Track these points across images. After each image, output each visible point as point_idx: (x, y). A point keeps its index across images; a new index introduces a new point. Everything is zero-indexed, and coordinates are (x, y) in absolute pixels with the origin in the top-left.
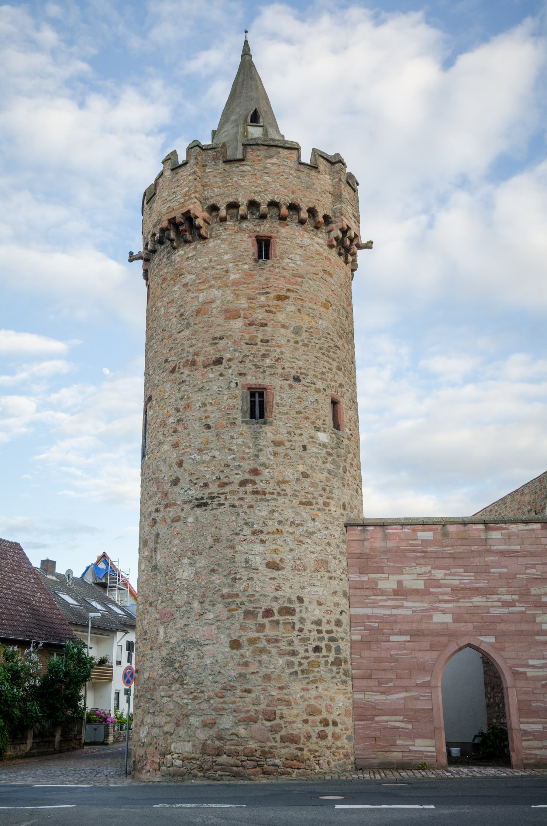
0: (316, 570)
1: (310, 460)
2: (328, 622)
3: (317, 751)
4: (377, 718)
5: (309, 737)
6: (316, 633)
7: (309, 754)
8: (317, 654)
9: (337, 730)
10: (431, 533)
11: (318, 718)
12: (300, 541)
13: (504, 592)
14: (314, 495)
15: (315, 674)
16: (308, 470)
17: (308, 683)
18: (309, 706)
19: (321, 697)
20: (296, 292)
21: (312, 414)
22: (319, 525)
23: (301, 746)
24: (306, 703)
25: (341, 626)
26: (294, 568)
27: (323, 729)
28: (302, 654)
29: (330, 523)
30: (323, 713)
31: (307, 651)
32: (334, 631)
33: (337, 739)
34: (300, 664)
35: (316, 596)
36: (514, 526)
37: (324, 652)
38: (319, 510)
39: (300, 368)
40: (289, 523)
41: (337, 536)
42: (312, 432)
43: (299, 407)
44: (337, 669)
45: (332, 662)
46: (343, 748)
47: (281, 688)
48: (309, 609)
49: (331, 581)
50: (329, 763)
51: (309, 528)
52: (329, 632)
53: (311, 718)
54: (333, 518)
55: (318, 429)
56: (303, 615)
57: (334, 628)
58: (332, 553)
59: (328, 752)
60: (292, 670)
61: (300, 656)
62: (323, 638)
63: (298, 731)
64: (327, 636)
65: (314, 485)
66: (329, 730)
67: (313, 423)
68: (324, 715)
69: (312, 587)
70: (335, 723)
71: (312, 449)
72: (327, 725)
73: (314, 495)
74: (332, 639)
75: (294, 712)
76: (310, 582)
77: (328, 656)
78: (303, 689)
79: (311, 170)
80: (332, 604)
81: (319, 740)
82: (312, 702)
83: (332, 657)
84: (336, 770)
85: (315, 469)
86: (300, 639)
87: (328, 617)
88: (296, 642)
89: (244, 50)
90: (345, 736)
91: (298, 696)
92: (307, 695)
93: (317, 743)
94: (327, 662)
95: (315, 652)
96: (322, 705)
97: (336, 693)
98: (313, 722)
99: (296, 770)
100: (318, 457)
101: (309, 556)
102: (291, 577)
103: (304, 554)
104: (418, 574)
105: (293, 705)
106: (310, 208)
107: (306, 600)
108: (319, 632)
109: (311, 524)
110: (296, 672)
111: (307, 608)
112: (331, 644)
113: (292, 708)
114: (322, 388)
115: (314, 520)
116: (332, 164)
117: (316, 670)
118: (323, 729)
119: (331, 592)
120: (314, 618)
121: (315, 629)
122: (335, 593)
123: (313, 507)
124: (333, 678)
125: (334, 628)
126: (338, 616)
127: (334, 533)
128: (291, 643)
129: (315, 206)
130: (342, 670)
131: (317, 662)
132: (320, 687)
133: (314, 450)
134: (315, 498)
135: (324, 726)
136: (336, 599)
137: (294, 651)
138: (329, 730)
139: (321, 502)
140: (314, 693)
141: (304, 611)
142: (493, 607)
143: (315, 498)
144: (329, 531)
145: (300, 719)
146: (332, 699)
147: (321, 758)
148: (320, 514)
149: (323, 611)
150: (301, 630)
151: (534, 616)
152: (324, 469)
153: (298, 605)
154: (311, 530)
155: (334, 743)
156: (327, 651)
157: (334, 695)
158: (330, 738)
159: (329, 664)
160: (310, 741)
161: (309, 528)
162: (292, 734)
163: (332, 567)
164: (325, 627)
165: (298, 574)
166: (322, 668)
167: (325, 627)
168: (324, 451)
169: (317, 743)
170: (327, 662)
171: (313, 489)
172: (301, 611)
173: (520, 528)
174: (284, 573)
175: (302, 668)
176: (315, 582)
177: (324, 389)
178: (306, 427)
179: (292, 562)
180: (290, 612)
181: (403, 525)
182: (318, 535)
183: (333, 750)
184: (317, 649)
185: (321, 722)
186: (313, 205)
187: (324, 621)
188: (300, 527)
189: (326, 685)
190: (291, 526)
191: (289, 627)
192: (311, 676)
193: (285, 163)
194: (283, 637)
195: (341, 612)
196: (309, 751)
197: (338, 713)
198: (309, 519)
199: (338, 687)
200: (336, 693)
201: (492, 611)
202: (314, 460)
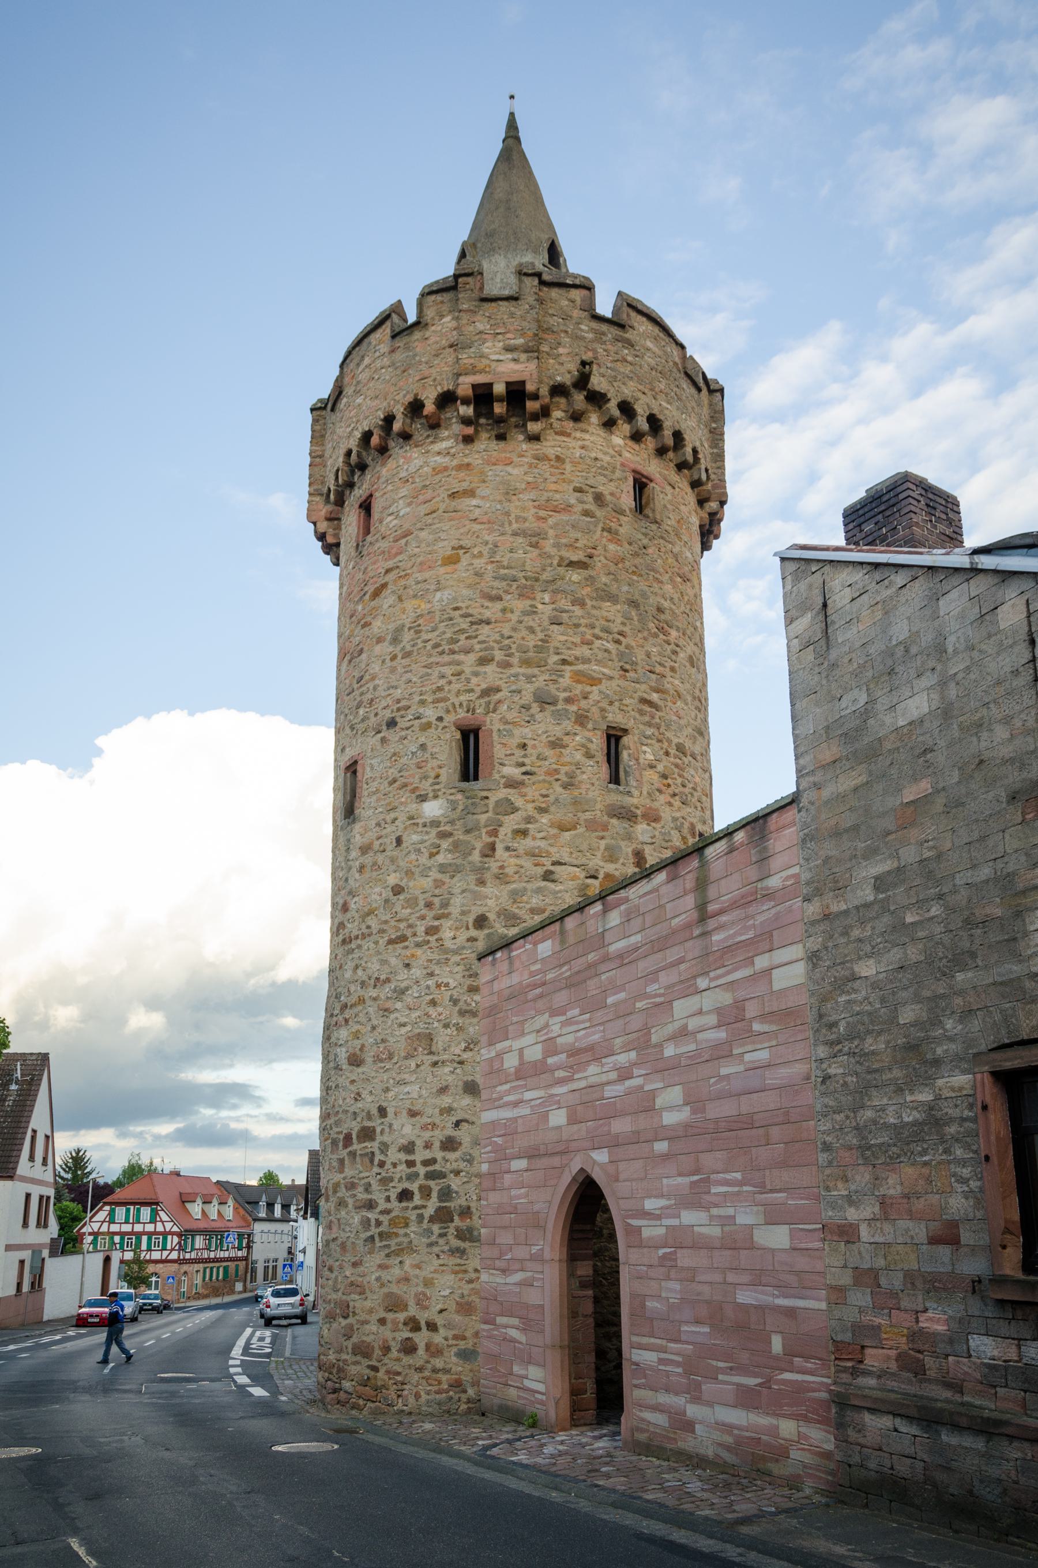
2: (428, 1146)
3: (399, 1374)
4: (500, 1320)
5: (386, 1349)
6: (403, 1167)
7: (386, 1377)
8: (404, 1204)
9: (438, 1339)
10: (549, 943)
11: (401, 1316)
12: (386, 1010)
13: (622, 1048)
17: (388, 1255)
18: (390, 1295)
21: (413, 776)
22: (417, 972)
23: (374, 1363)
24: (385, 1290)
25: (454, 1149)
28: (382, 1205)
29: (438, 963)
30: (410, 1308)
31: (388, 1199)
32: (439, 1159)
34: (378, 1223)
37: (417, 1200)
39: (398, 701)
41: (452, 984)
42: (413, 807)
43: (393, 773)
44: (440, 1228)
45: (431, 1217)
48: (395, 1127)
50: (417, 1396)
52: (426, 1163)
53: (390, 1316)
54: (446, 951)
55: (423, 798)
56: (386, 1138)
57: (439, 1155)
59: (416, 1377)
61: (379, 1209)
62: (416, 1175)
63: (372, 1337)
64: (422, 1170)
65: (412, 902)
66: (421, 1338)
68: (413, 1311)
70: (432, 1327)
71: (412, 838)
72: (416, 1328)
74: (431, 1176)
75: (368, 1304)
77: (424, 1207)
78: (380, 1266)
80: (437, 1110)
81: (401, 1355)
82: (394, 1289)
83: (432, 1205)
84: (430, 1410)
86: (380, 1180)
87: (427, 1135)
88: (375, 1186)
90: (454, 1350)
91: (373, 1277)
92: (385, 1276)
93: (398, 1360)
94: (421, 1217)
95: (400, 1201)
96: (409, 1293)
97: (435, 1271)
98: (395, 1322)
99: (369, 1404)
100: (419, 850)
101: (397, 1033)
102: (373, 1074)
104: (538, 1031)
105: (368, 1293)
106: (410, 403)
107: (390, 1111)
108: (410, 1164)
110: (372, 1237)
111: (390, 1126)
114: (433, 719)
115: (407, 966)
117: (401, 1231)
119: (434, 1090)
120: (402, 1141)
121: (404, 1159)
122: (443, 1090)
123: (406, 944)
124: (430, 1245)
125: (439, 1155)
126: (450, 1132)
127: (445, 981)
128: (368, 1188)
129: (416, 395)
130: (452, 1231)
131: (403, 1218)
132: (408, 1262)
133: (415, 838)
134: (410, 926)
135: (412, 1330)
136: (446, 1100)
137: (371, 1200)
138: (421, 1338)
139: (421, 929)
140: (397, 1272)
142: (608, 1083)
143: (410, 926)
145: (375, 1317)
146: (428, 1283)
147: (405, 1386)
148: (419, 952)
149: (418, 1126)
150: (382, 1164)
151: (653, 1094)
152: (430, 868)
154: (403, 985)
155: (428, 1362)
157: (432, 1275)
158: (421, 1351)
159: (426, 1221)
160: (389, 1355)
162: (363, 1342)
163: (439, 1044)
164: (420, 1155)
165: (381, 1068)
166: (413, 1227)
167: (420, 1155)
168: (434, 832)
169: (398, 1360)
170: (421, 1217)
171: (409, 911)
172: (382, 1132)
173: (642, 892)
174: (364, 1069)
175: (381, 1229)
176: (406, 1076)
178: (402, 803)
180: (367, 1134)
181: (524, 937)
182: (414, 992)
183: (427, 1373)
184: (405, 1195)
185: (405, 1324)
187: (419, 1143)
188: (387, 985)
191: (367, 1160)
192: (393, 1243)
193: (377, 354)
194: (360, 1179)
195: (457, 1124)
196: (388, 1372)
197: (439, 1307)
198: (401, 966)
199: (441, 1262)
200: (435, 1271)
201: (610, 1091)
202: (413, 857)
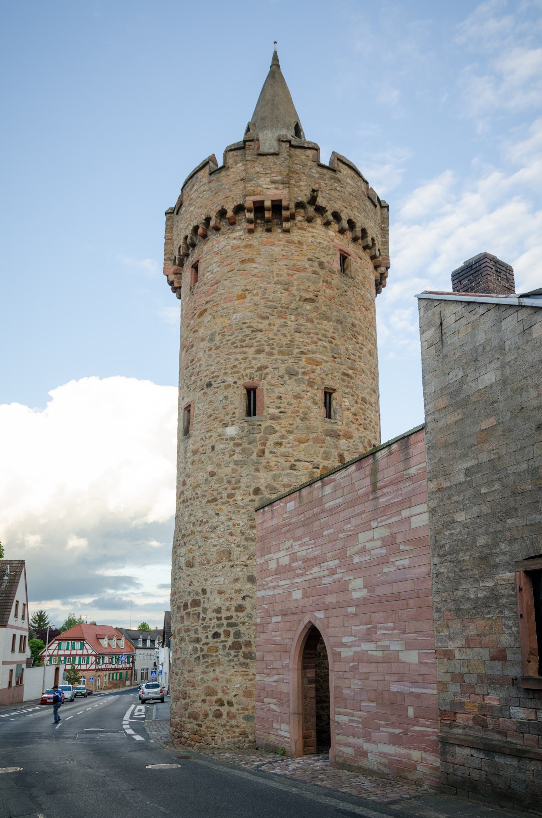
0: (218, 562)
1: (217, 458)
2: (228, 609)
3: (213, 728)
4: (266, 700)
5: (206, 715)
7: (206, 730)
8: (216, 640)
9: (233, 710)
11: (214, 698)
12: (206, 538)
14: (219, 491)
15: (213, 658)
16: (214, 468)
17: (207, 667)
18: (208, 687)
19: (217, 679)
20: (213, 300)
21: (221, 413)
22: (222, 518)
23: (199, 722)
24: (206, 685)
25: (242, 611)
26: (202, 564)
27: (219, 708)
28: (204, 640)
29: (234, 513)
30: (218, 694)
32: (234, 617)
33: (231, 718)
34: (202, 650)
35: (217, 586)
36: (338, 475)
37: (222, 638)
38: (223, 503)
39: (213, 373)
40: (199, 523)
43: (210, 411)
44: (235, 652)
45: (230, 646)
46: (237, 726)
47: (189, 671)
48: (211, 599)
49: (232, 569)
50: (222, 739)
51: (213, 524)
52: (227, 618)
53: (208, 698)
54: (239, 507)
55: (226, 425)
56: (206, 605)
57: (234, 614)
58: (236, 542)
59: (222, 730)
60: (197, 655)
62: (222, 624)
63: (198, 709)
64: (225, 622)
65: (220, 481)
66: (224, 710)
67: (221, 421)
68: (220, 695)
69: (215, 578)
70: (230, 704)
71: (220, 446)
72: (222, 704)
73: (219, 491)
75: (196, 692)
76: (212, 574)
77: (226, 641)
78: (203, 672)
79: (220, 173)
80: (233, 591)
81: (214, 718)
82: (210, 684)
83: (231, 640)
84: (229, 746)
85: (221, 465)
86: (203, 627)
87: (228, 604)
88: (200, 630)
89: (274, 56)
90: (242, 715)
91: (199, 678)
92: (206, 677)
93: (212, 721)
94: (224, 647)
96: (218, 686)
97: (232, 675)
98: (210, 701)
99: (197, 744)
103: (208, 549)
104: (287, 549)
105: (196, 687)
107: (208, 591)
108: (219, 619)
109: (215, 519)
110: (199, 657)
111: (208, 599)
112: (230, 629)
113: (195, 689)
115: (218, 514)
116: (243, 148)
117: (214, 654)
118: (219, 708)
119: (232, 580)
120: (214, 607)
122: (236, 580)
123: (217, 503)
124: (230, 661)
125: (234, 614)
128: (196, 631)
129: (223, 206)
130: (241, 653)
132: (217, 670)
133: (222, 446)
134: (219, 493)
136: (238, 586)
137: (198, 638)
138: (224, 710)
139: (225, 495)
140: (212, 675)
141: (207, 601)
142: (324, 576)
143: (219, 493)
144: (233, 521)
146: (228, 681)
148: (224, 507)
149: (223, 599)
150: (204, 619)
153: (202, 596)
155: (228, 722)
156: (225, 636)
158: (224, 716)
159: (227, 649)
161: (213, 524)
162: (194, 711)
163: (234, 556)
164: (224, 614)
166: (220, 652)
169: (212, 721)
170: (224, 647)
171: (218, 485)
172: (204, 602)
176: (217, 573)
177: (235, 383)
178: (214, 428)
179: (200, 558)
180: (196, 603)
182: (221, 528)
183: (227, 728)
184: (216, 635)
185: (216, 702)
186: (220, 207)
187: (224, 608)
188: (207, 524)
189: (223, 667)
190: (200, 525)
191: (196, 617)
192: (210, 660)
194: (192, 627)
195: (244, 598)
196: (207, 727)
197: (234, 693)
198: (214, 514)
199: (235, 670)
201: (324, 581)
202: (221, 456)
